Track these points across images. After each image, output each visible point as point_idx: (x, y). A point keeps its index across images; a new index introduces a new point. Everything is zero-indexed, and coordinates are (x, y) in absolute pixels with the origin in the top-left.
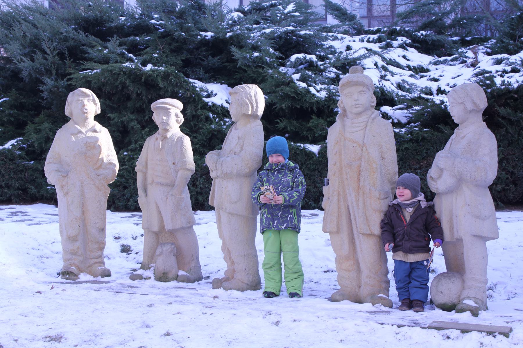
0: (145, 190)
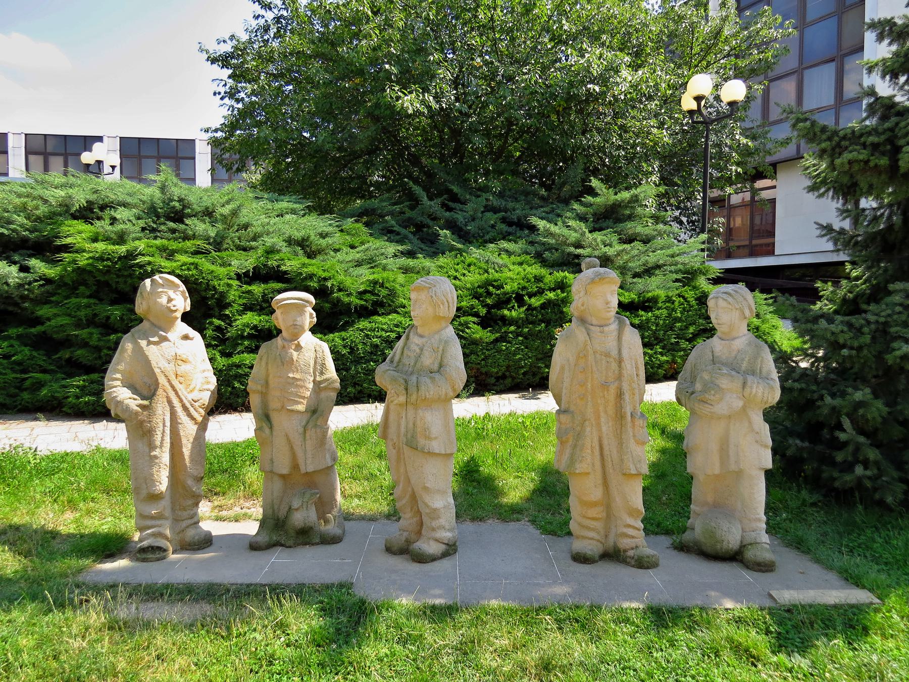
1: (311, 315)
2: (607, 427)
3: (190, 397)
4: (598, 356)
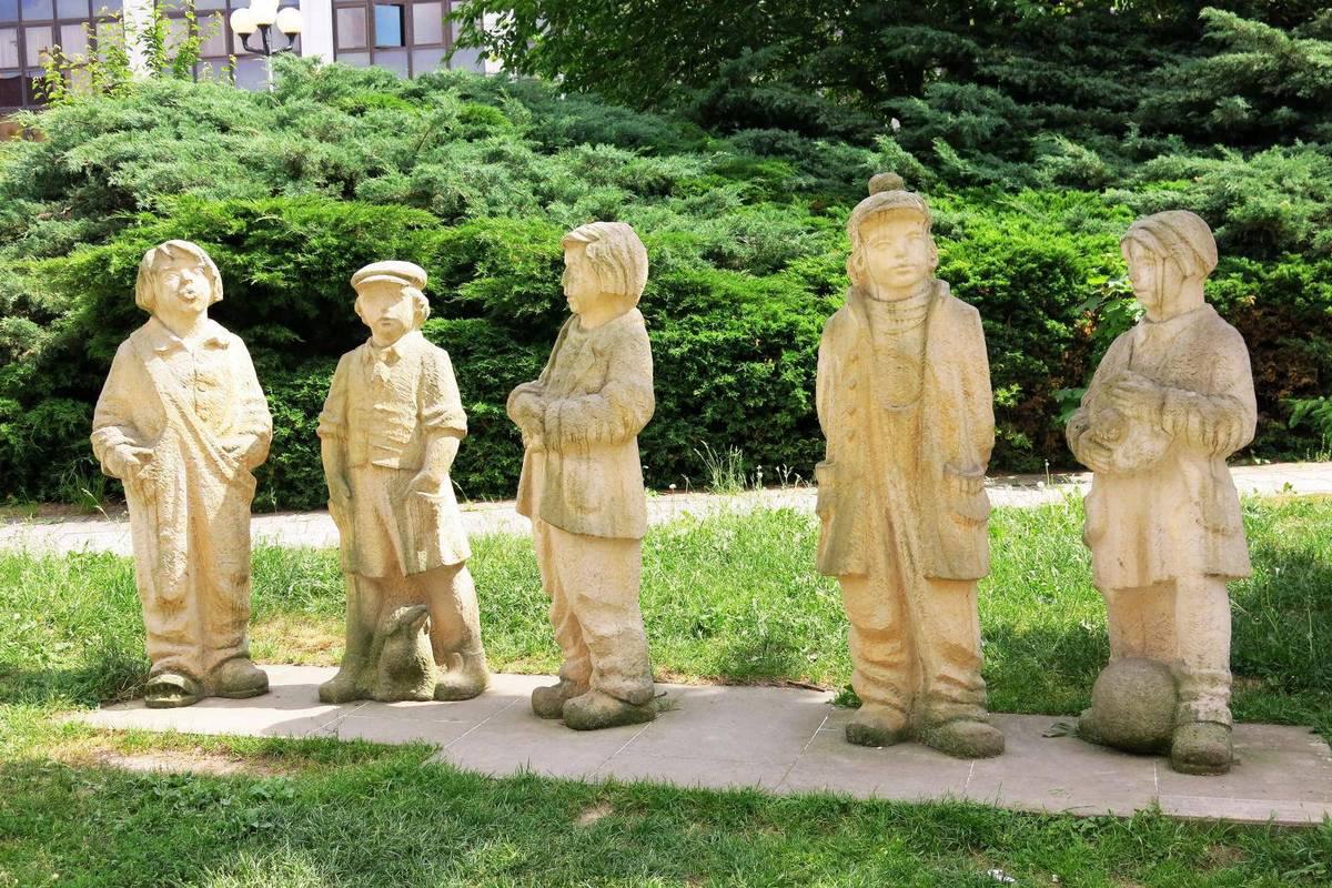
0: (345, 475)
1: (417, 301)
2: (898, 493)
3: (219, 444)
4: (881, 357)
